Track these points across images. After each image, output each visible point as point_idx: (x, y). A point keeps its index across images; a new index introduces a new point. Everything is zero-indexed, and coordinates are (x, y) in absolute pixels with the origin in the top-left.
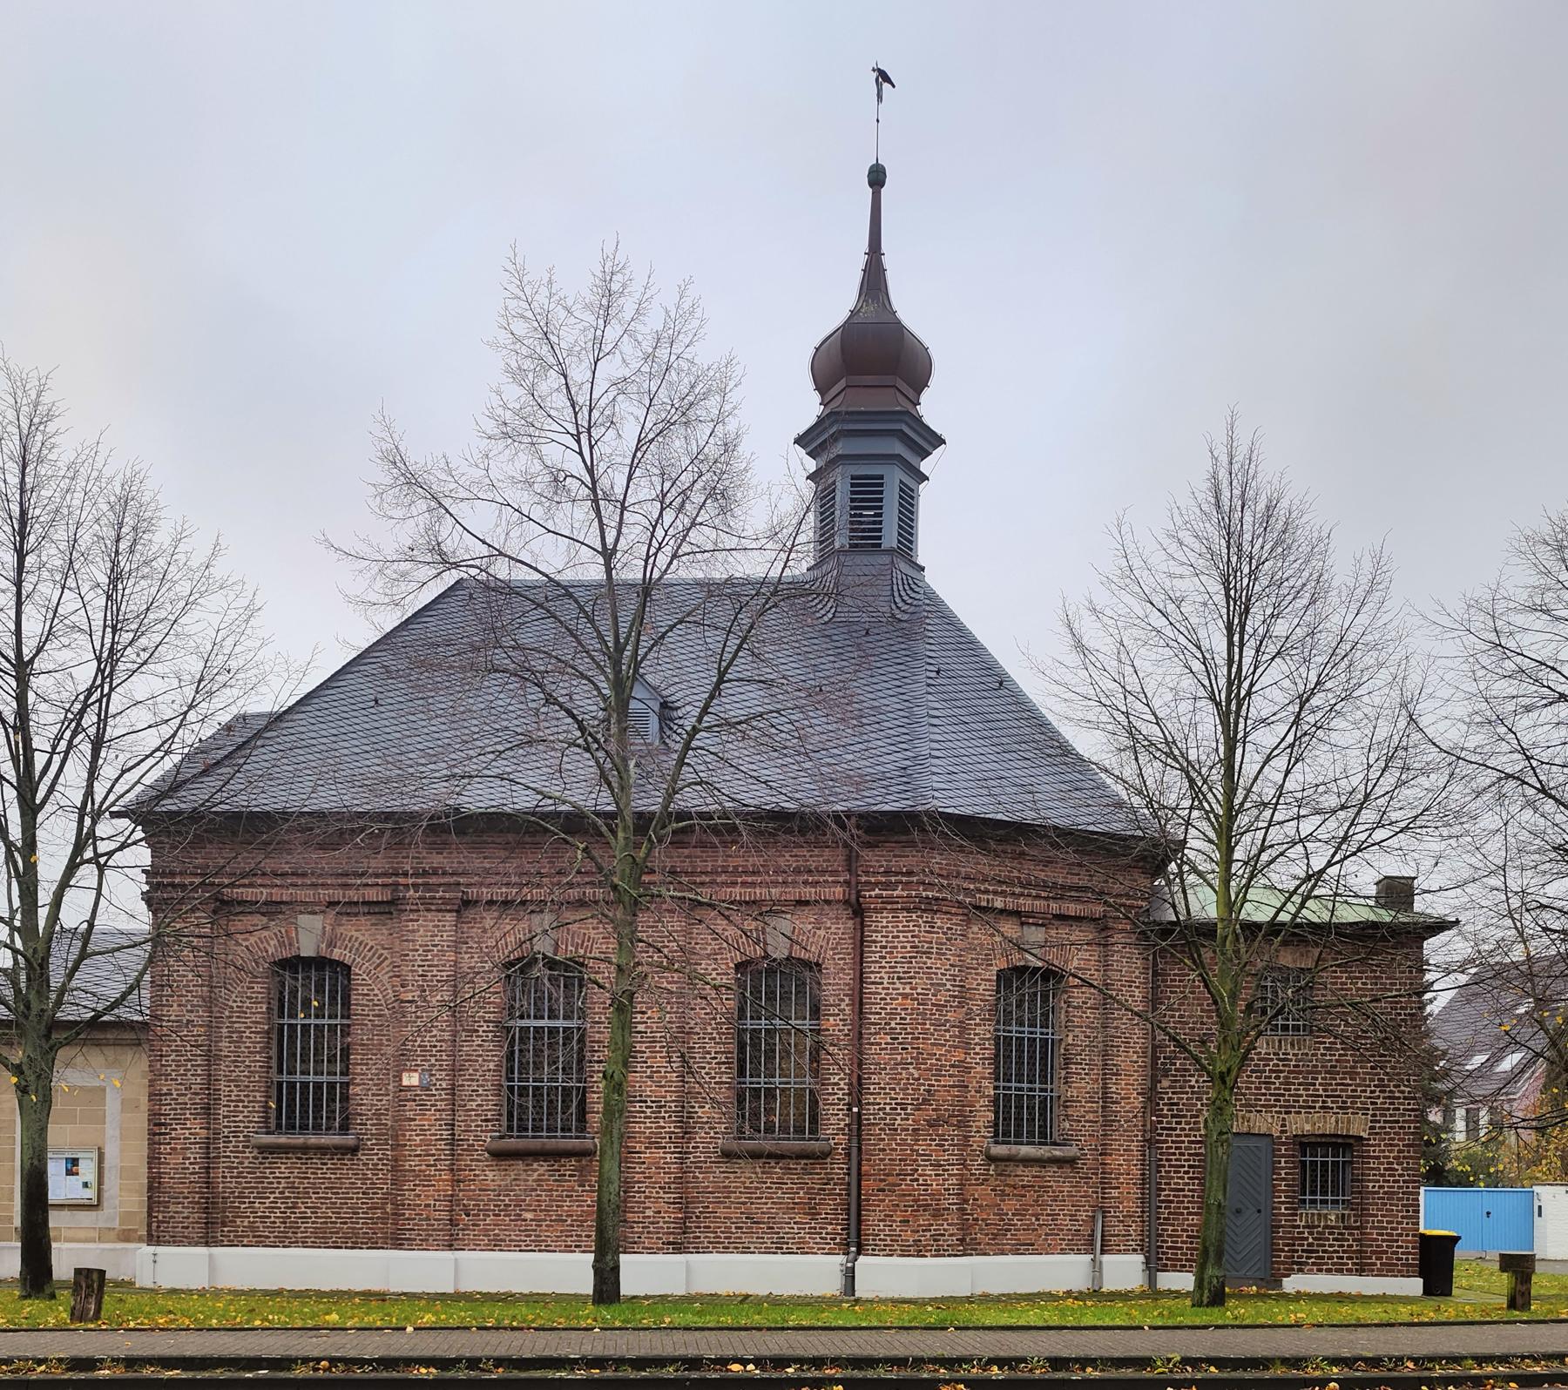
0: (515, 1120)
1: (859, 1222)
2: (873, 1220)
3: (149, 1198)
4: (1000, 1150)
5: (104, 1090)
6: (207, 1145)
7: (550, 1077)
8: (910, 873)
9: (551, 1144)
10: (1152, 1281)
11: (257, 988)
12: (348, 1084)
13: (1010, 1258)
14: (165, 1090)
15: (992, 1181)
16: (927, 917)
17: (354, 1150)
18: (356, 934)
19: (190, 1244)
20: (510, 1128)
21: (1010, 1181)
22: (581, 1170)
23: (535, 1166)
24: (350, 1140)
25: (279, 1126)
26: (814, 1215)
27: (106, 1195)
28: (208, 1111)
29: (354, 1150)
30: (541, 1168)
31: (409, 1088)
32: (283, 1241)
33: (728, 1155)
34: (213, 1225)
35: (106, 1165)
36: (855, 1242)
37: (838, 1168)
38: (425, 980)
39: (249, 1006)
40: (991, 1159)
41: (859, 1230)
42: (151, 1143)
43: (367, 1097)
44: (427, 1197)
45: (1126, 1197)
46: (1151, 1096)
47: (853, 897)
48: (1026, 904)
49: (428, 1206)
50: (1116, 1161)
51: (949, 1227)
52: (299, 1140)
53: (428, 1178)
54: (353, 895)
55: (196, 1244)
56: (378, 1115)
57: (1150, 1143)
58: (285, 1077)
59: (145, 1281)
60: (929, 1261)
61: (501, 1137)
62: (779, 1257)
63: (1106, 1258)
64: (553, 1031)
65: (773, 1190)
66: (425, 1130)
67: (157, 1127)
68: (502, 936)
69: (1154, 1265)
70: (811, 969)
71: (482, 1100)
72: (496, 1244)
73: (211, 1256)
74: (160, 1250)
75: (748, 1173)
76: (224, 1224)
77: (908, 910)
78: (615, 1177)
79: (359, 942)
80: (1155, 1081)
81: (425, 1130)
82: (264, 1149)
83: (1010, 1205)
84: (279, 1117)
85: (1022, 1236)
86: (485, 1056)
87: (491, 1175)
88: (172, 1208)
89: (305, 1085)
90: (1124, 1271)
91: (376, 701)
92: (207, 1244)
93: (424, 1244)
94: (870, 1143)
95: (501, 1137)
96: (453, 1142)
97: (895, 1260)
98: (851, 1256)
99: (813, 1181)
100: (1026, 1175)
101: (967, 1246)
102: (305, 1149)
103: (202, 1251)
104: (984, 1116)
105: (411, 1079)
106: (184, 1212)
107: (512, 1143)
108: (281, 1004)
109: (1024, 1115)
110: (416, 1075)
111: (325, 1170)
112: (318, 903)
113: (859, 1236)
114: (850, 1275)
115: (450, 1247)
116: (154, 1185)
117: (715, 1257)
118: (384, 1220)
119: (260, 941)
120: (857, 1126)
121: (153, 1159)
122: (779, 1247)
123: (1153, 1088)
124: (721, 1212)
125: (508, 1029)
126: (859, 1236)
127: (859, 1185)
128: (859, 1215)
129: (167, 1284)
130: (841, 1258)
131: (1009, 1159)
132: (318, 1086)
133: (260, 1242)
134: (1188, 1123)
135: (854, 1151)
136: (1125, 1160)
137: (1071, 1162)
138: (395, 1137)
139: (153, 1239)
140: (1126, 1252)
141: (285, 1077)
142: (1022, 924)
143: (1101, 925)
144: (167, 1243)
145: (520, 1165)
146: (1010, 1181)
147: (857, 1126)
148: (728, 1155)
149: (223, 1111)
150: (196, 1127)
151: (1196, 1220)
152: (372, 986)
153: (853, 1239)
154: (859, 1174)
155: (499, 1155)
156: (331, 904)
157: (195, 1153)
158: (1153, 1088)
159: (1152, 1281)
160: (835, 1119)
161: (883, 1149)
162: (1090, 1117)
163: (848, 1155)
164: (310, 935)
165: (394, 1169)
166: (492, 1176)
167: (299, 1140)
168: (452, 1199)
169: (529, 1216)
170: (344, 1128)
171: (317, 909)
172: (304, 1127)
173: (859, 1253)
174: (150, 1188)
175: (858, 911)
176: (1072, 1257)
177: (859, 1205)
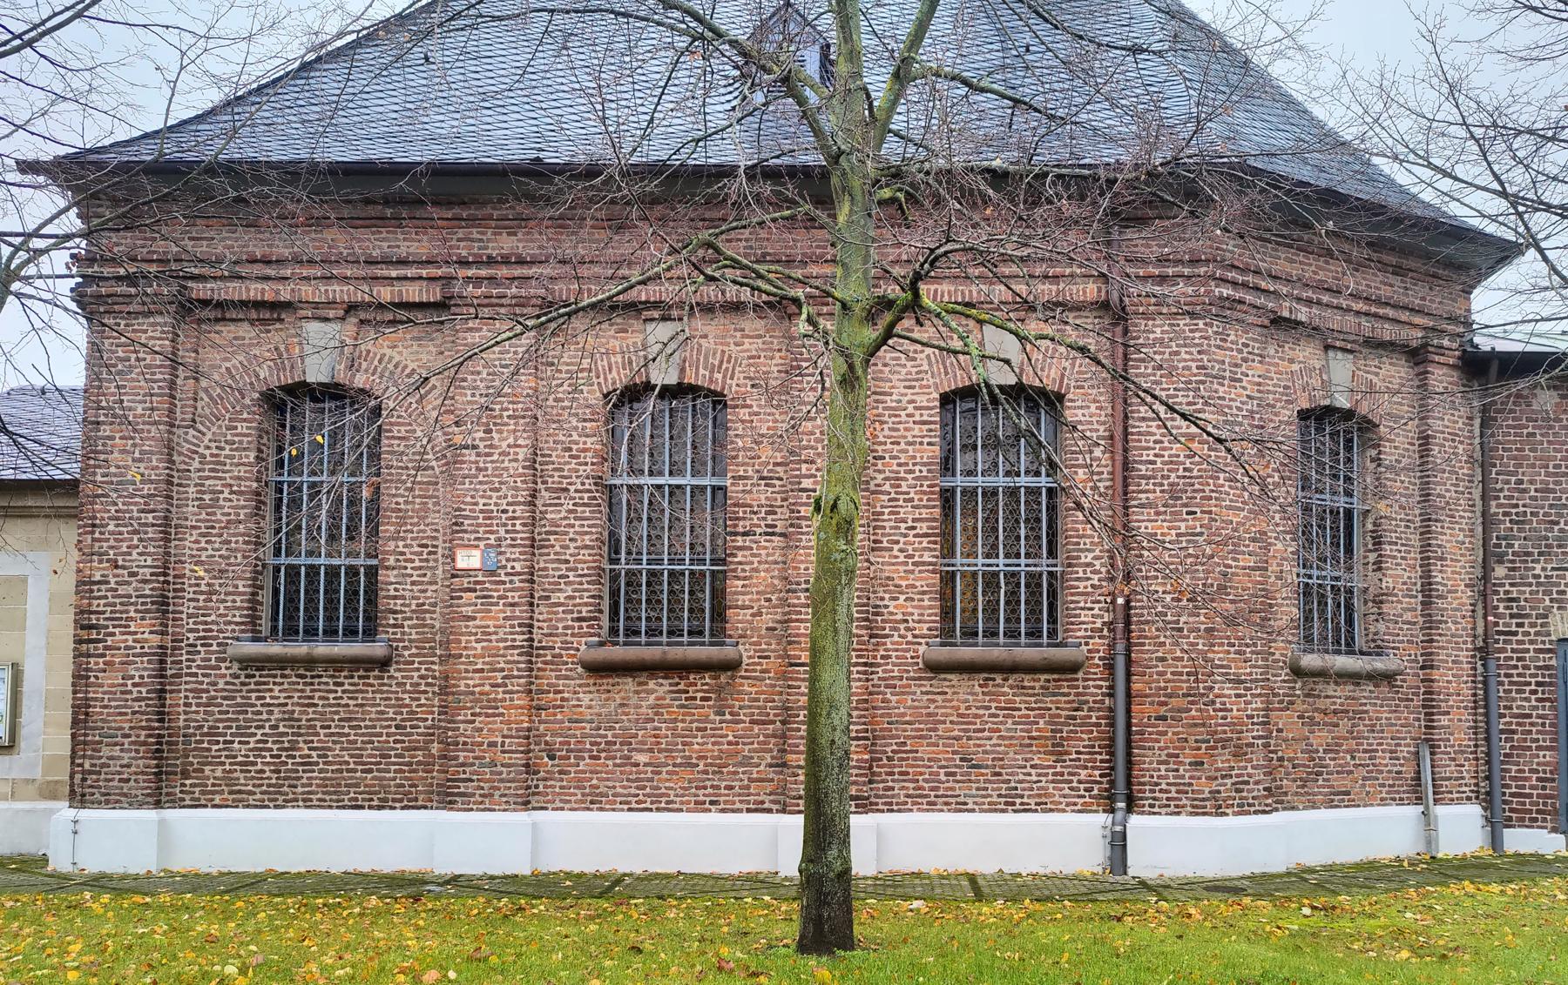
0: (621, 624)
1: (1129, 764)
2: (1150, 762)
3: (73, 736)
4: (1310, 661)
5: (23, 580)
6: (161, 657)
7: (676, 554)
8: (1195, 262)
9: (677, 653)
10: (1496, 841)
11: (242, 428)
12: (376, 568)
13: (1323, 814)
14: (97, 578)
15: (1299, 706)
16: (1217, 326)
17: (384, 664)
18: (388, 352)
19: (131, 805)
20: (614, 631)
21: (1321, 704)
22: (719, 690)
23: (652, 684)
24: (377, 649)
25: (274, 629)
26: (1059, 753)
27: (24, 732)
28: (163, 606)
29: (384, 664)
30: (660, 687)
31: (467, 572)
32: (276, 797)
33: (936, 668)
34: (167, 777)
35: (26, 687)
36: (1122, 792)
37: (1093, 687)
38: (491, 455)
39: (227, 450)
40: (1297, 672)
41: (1129, 776)
42: (78, 655)
43: (404, 586)
44: (493, 731)
45: (1457, 726)
46: (1484, 587)
47: (1115, 295)
48: (1335, 320)
49: (492, 744)
50: (1444, 677)
51: (1253, 769)
52: (300, 649)
53: (493, 704)
54: (386, 294)
55: (140, 806)
56: (420, 611)
57: (1484, 652)
58: (283, 560)
59: (60, 862)
60: (1231, 821)
61: (602, 644)
62: (1010, 817)
63: (1440, 810)
64: (675, 490)
65: (992, 716)
66: (489, 633)
67: (87, 631)
68: (613, 354)
69: (1495, 825)
70: (1033, 408)
71: (573, 589)
72: (594, 801)
73: (162, 822)
74: (85, 814)
75: (965, 691)
76: (185, 774)
77: (1192, 315)
78: (841, 697)
79: (393, 359)
80: (1486, 568)
81: (489, 633)
82: (247, 663)
83: (1321, 738)
84: (275, 618)
85: (1340, 783)
86: (577, 535)
87: (586, 699)
88: (106, 751)
89: (313, 571)
90: (1461, 828)
91: (427, 59)
92: (158, 804)
93: (486, 803)
94: (1145, 652)
95: (602, 644)
96: (530, 650)
97: (1184, 820)
98: (1119, 815)
99: (1057, 705)
100: (1338, 694)
101: (1275, 799)
102: (310, 662)
103: (150, 815)
104: (1287, 611)
105: (469, 559)
106: (125, 757)
107: (618, 653)
108: (276, 454)
109: (1333, 614)
110: (477, 553)
111: (336, 693)
112: (331, 303)
113: (1129, 784)
114: (1118, 843)
115: (526, 805)
116: (81, 717)
117: (916, 817)
118: (427, 766)
119: (241, 359)
120: (1124, 622)
121: (81, 678)
122: (1011, 803)
123: (1485, 578)
124: (924, 751)
125: (611, 488)
126: (1129, 784)
127: (1128, 711)
128: (1129, 754)
129: (93, 866)
130: (1102, 819)
131: (1322, 674)
132: (333, 572)
133: (239, 799)
134: (1533, 625)
135: (1120, 662)
136: (1454, 676)
137: (1388, 677)
138: (446, 644)
139: (79, 798)
140: (1459, 801)
141: (283, 560)
142: (1327, 348)
143: (1417, 356)
144: (98, 804)
145: (629, 684)
146: (1321, 704)
147: (1124, 622)
148: (936, 668)
149: (187, 608)
150: (144, 632)
151: (1549, 756)
152: (409, 430)
153: (1121, 788)
154: (1128, 695)
155: (598, 670)
156: (351, 308)
157: (142, 669)
158: (1485, 578)
159: (1496, 841)
160: (1086, 620)
161: (1163, 657)
162: (1408, 616)
163: (1110, 668)
164: (319, 352)
165: (444, 691)
166: (588, 700)
167: (300, 649)
168: (528, 735)
169: (642, 758)
170: (370, 634)
171: (331, 314)
172: (311, 633)
173: (1129, 810)
174: (75, 722)
175: (1114, 313)
176: (1394, 810)
177: (1129, 742)
